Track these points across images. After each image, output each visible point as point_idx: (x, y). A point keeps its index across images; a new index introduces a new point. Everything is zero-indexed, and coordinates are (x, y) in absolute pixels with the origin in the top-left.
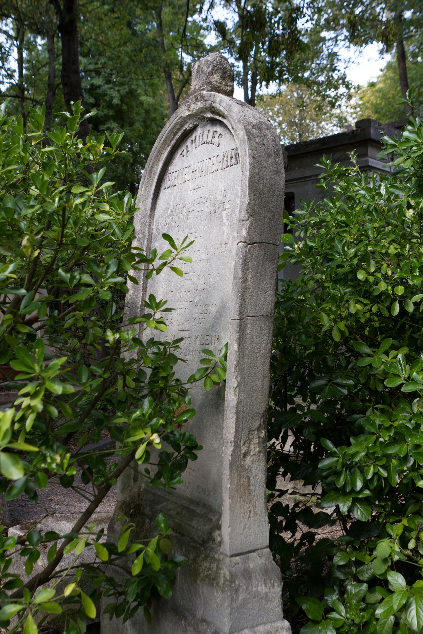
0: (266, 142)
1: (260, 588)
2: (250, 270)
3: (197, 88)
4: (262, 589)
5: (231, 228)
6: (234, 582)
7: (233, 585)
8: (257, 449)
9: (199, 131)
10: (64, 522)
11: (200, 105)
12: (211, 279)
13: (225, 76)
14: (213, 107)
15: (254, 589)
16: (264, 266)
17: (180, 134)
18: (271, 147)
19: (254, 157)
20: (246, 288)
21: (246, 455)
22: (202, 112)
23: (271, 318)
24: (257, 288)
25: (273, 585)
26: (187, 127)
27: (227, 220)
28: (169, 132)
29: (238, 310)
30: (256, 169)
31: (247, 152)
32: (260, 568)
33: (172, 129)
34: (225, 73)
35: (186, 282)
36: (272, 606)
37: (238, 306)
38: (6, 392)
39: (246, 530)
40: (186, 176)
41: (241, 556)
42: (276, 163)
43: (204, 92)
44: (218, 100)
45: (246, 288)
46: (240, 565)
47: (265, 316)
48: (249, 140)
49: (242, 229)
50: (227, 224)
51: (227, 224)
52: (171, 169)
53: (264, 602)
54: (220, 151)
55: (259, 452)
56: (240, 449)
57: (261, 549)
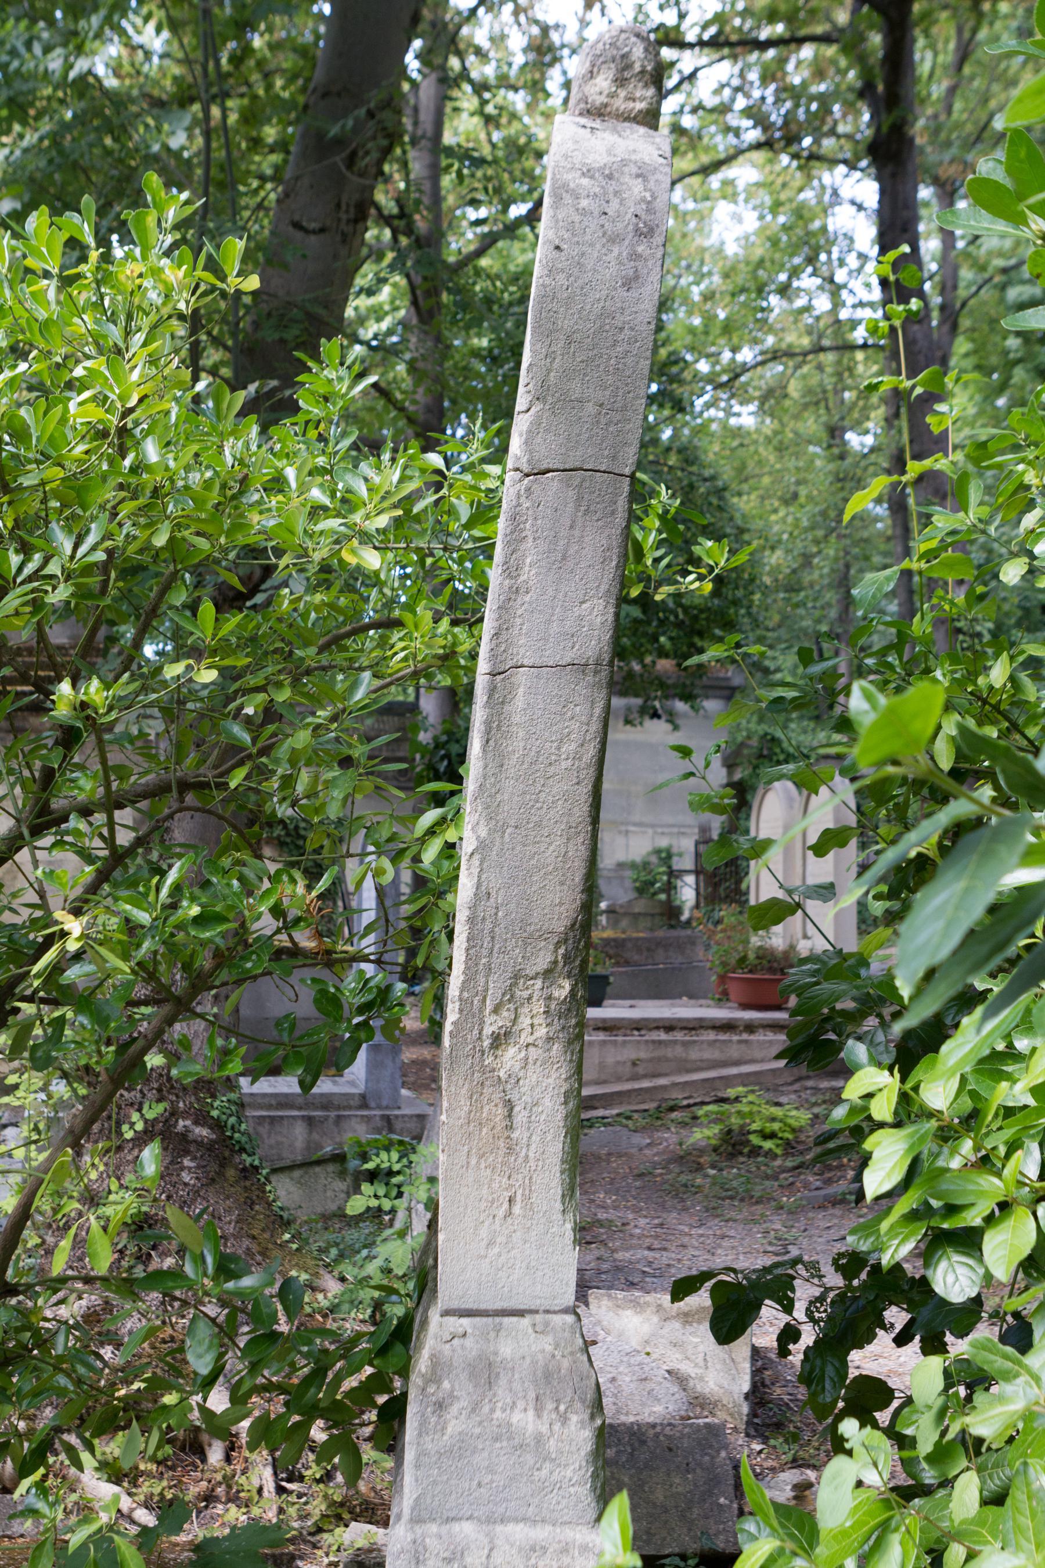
0: (612, 209)
1: (516, 1417)
4: (525, 1420)
6: (438, 1382)
7: (431, 1389)
8: (542, 1032)
10: (629, 1312)
13: (626, 74)
15: (498, 1414)
16: (577, 533)
21: (498, 1041)
23: (596, 672)
24: (551, 592)
25: (564, 1420)
32: (534, 1363)
34: (629, 66)
36: (555, 1477)
38: (745, 1036)
39: (496, 1250)
41: (477, 1320)
42: (635, 256)
46: (468, 1342)
47: (580, 667)
53: (530, 1459)
55: (549, 1039)
56: (482, 1022)
57: (547, 1312)
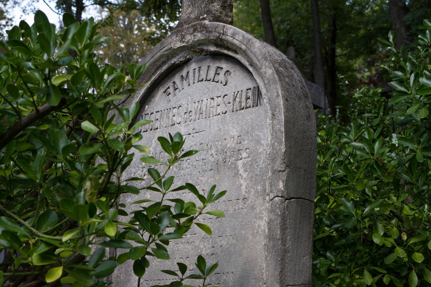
2: (289, 230)
3: (193, 16)
5: (251, 181)
9: (193, 66)
11: (199, 36)
12: (224, 243)
14: (221, 40)
17: (165, 68)
18: (300, 88)
19: (287, 100)
20: (286, 251)
22: (200, 44)
26: (175, 60)
27: (245, 171)
28: (151, 65)
29: (278, 278)
30: (290, 113)
31: (280, 93)
33: (155, 62)
35: (181, 246)
37: (277, 273)
40: (174, 118)
43: (207, 22)
44: (230, 32)
45: (286, 251)
48: (280, 80)
49: (278, 182)
50: (245, 175)
51: (245, 175)
52: (148, 108)
54: (230, 90)
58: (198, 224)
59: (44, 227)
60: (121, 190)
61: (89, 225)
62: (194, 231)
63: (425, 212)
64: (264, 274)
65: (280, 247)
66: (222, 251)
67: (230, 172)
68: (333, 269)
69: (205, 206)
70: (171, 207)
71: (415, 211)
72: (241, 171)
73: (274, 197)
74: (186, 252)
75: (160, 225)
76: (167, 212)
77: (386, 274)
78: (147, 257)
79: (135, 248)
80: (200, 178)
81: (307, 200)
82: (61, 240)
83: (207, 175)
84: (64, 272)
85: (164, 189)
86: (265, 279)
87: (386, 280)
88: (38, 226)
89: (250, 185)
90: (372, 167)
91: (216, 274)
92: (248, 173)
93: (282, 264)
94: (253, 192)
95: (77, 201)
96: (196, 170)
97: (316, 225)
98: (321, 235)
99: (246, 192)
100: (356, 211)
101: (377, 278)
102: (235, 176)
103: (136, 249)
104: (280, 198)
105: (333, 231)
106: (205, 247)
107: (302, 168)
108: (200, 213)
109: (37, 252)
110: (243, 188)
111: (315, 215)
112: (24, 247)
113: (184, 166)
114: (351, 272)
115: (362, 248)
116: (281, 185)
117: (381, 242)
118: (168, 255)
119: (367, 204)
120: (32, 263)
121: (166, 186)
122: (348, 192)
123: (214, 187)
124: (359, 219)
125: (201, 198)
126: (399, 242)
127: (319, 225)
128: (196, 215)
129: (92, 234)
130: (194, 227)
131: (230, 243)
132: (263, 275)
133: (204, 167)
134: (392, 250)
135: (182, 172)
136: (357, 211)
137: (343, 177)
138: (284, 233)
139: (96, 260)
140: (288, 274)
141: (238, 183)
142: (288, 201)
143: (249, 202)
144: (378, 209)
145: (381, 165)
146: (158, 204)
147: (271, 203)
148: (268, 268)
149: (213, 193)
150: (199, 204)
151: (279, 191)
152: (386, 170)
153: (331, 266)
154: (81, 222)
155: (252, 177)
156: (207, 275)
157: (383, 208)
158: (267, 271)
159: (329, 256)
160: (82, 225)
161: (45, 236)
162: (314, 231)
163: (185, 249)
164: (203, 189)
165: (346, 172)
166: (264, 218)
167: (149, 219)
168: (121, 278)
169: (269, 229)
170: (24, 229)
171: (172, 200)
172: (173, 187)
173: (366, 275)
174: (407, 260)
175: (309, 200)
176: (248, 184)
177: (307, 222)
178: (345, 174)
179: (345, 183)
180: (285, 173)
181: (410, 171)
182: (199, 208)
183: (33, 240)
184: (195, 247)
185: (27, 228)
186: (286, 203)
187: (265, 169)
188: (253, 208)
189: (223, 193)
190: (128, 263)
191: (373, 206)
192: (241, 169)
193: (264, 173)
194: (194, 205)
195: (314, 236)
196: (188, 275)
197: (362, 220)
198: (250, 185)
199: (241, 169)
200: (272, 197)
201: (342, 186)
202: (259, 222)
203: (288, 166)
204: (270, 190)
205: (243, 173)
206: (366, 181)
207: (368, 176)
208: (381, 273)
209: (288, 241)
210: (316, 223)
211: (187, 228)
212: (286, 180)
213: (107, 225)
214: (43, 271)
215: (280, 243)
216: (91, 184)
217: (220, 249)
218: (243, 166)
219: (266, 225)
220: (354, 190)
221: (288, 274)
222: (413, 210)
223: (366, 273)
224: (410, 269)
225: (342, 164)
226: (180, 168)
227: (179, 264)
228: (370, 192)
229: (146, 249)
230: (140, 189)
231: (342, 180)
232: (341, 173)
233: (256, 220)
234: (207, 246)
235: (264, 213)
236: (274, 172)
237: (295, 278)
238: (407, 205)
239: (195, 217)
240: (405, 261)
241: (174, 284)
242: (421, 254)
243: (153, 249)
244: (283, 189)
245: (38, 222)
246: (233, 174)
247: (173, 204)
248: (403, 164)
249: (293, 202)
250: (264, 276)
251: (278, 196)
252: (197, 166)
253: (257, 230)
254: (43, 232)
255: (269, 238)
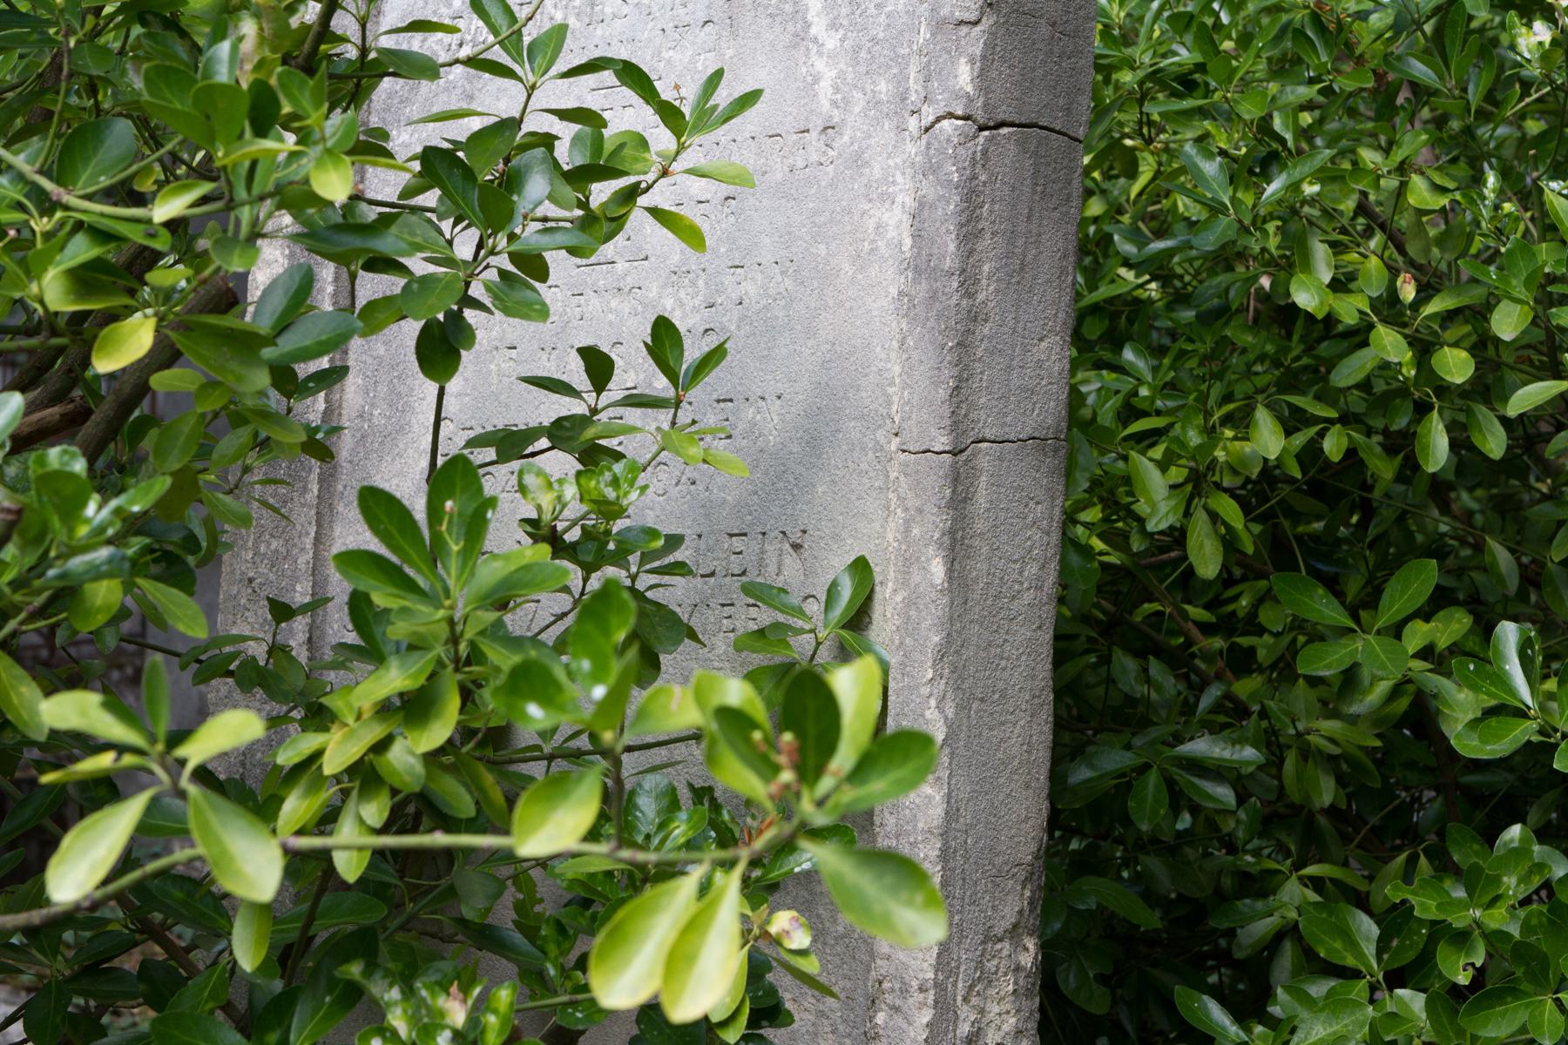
5: (855, 61)
12: (750, 289)
20: (975, 317)
27: (833, 26)
37: (943, 393)
45: (975, 317)
58: (655, 212)
59: (84, 178)
60: (370, 70)
61: (254, 164)
62: (640, 249)
63: (1485, 198)
64: (896, 399)
65: (954, 301)
66: (742, 319)
67: (778, 29)
68: (1145, 406)
69: (681, 148)
70: (557, 138)
71: (1450, 196)
72: (818, 28)
73: (938, 120)
74: (611, 324)
75: (515, 198)
76: (539, 152)
77: (1331, 422)
78: (470, 315)
79: (423, 277)
80: (666, 55)
81: (1059, 132)
82: (149, 221)
83: (693, 43)
84: (160, 340)
85: (533, 70)
86: (897, 419)
87: (1333, 446)
88: (61, 170)
89: (850, 76)
90: (1299, 33)
91: (718, 401)
92: (841, 32)
93: (959, 361)
94: (862, 103)
95: (208, 75)
96: (651, 25)
97: (1088, 260)
98: (1104, 292)
99: (834, 103)
100: (1235, 192)
101: (1299, 440)
102: (795, 46)
103: (426, 280)
104: (960, 122)
105: (1148, 282)
106: (682, 305)
107: (1041, 16)
108: (665, 173)
109: (59, 263)
110: (825, 88)
111: (1084, 222)
112: (12, 241)
113: (608, 10)
114: (1208, 414)
115: (1250, 339)
116: (965, 76)
117: (1322, 303)
118: (544, 304)
119: (1274, 169)
120: (42, 302)
121: (539, 60)
122: (1208, 125)
123: (718, 75)
124: (1247, 222)
125: (669, 114)
126: (1389, 307)
127: (1096, 261)
128: (650, 177)
129: (262, 198)
130: (638, 220)
131: (772, 292)
132: (889, 404)
133: (682, 11)
134: (1359, 336)
135: (599, 32)
136: (1239, 195)
137: (1191, 73)
138: (971, 252)
139: (280, 309)
140: (983, 400)
141: (804, 70)
142: (986, 133)
143: (846, 138)
144: (1316, 188)
145: (1332, 27)
146: (509, 125)
147: (924, 142)
148: (909, 376)
149: (711, 103)
150: (661, 139)
151: (957, 97)
152: (1350, 46)
153: (1136, 394)
154: (220, 154)
155: (856, 49)
156: (686, 388)
157: (1335, 187)
158: (905, 386)
159: (1131, 363)
160: (226, 161)
161: (86, 205)
162: (1080, 279)
163: (601, 298)
164: (678, 79)
165: (1204, 53)
166: (899, 199)
167: (474, 177)
168: (375, 420)
169: (917, 236)
170: (11, 182)
171: (564, 115)
172: (562, 65)
173: (1261, 422)
174: (1413, 372)
175: (1064, 134)
176: (841, 75)
177: (1056, 214)
178: (1200, 59)
179: (1201, 91)
180: (979, 28)
181: (1438, 48)
182: (658, 154)
183: (45, 220)
184: (645, 306)
185: (20, 177)
186: (981, 140)
187: (905, 19)
188: (858, 161)
189: (750, 99)
190: (401, 367)
191: (1297, 173)
192: (816, 20)
193: (901, 33)
194: (643, 143)
195: (1078, 296)
196: (620, 395)
197: (1254, 223)
198: (850, 76)
199: (816, 20)
200: (931, 118)
201: (1188, 103)
202: (878, 214)
203: (990, 5)
204: (922, 96)
205: (824, 33)
206: (1273, 87)
207: (1284, 68)
208: (1317, 420)
209: (984, 282)
210: (1088, 253)
211: (614, 224)
212: (984, 57)
213: (320, 163)
214: (84, 331)
215: (955, 285)
216: (261, 29)
217: (736, 312)
218: (824, 8)
219: (906, 220)
220: (1229, 117)
221: (983, 400)
222: (1443, 190)
223: (1262, 416)
224: (1423, 409)
225: (1188, 26)
226: (591, 16)
227: (581, 351)
228: (1287, 128)
229: (468, 285)
230: (443, 65)
231: (1186, 83)
232: (1184, 55)
233: (867, 206)
234: (689, 303)
235: (899, 179)
236: (939, 25)
237: (1006, 415)
238: (1422, 173)
239: (643, 185)
240: (1406, 378)
241: (566, 424)
242: (1464, 354)
243: (488, 287)
244: (969, 89)
245: (61, 159)
246: (787, 38)
247: (566, 131)
248: (1413, 21)
249: (1007, 137)
250: (895, 408)
251: (951, 115)
252: (655, 9)
253: (873, 241)
254: (81, 193)
255: (917, 271)
